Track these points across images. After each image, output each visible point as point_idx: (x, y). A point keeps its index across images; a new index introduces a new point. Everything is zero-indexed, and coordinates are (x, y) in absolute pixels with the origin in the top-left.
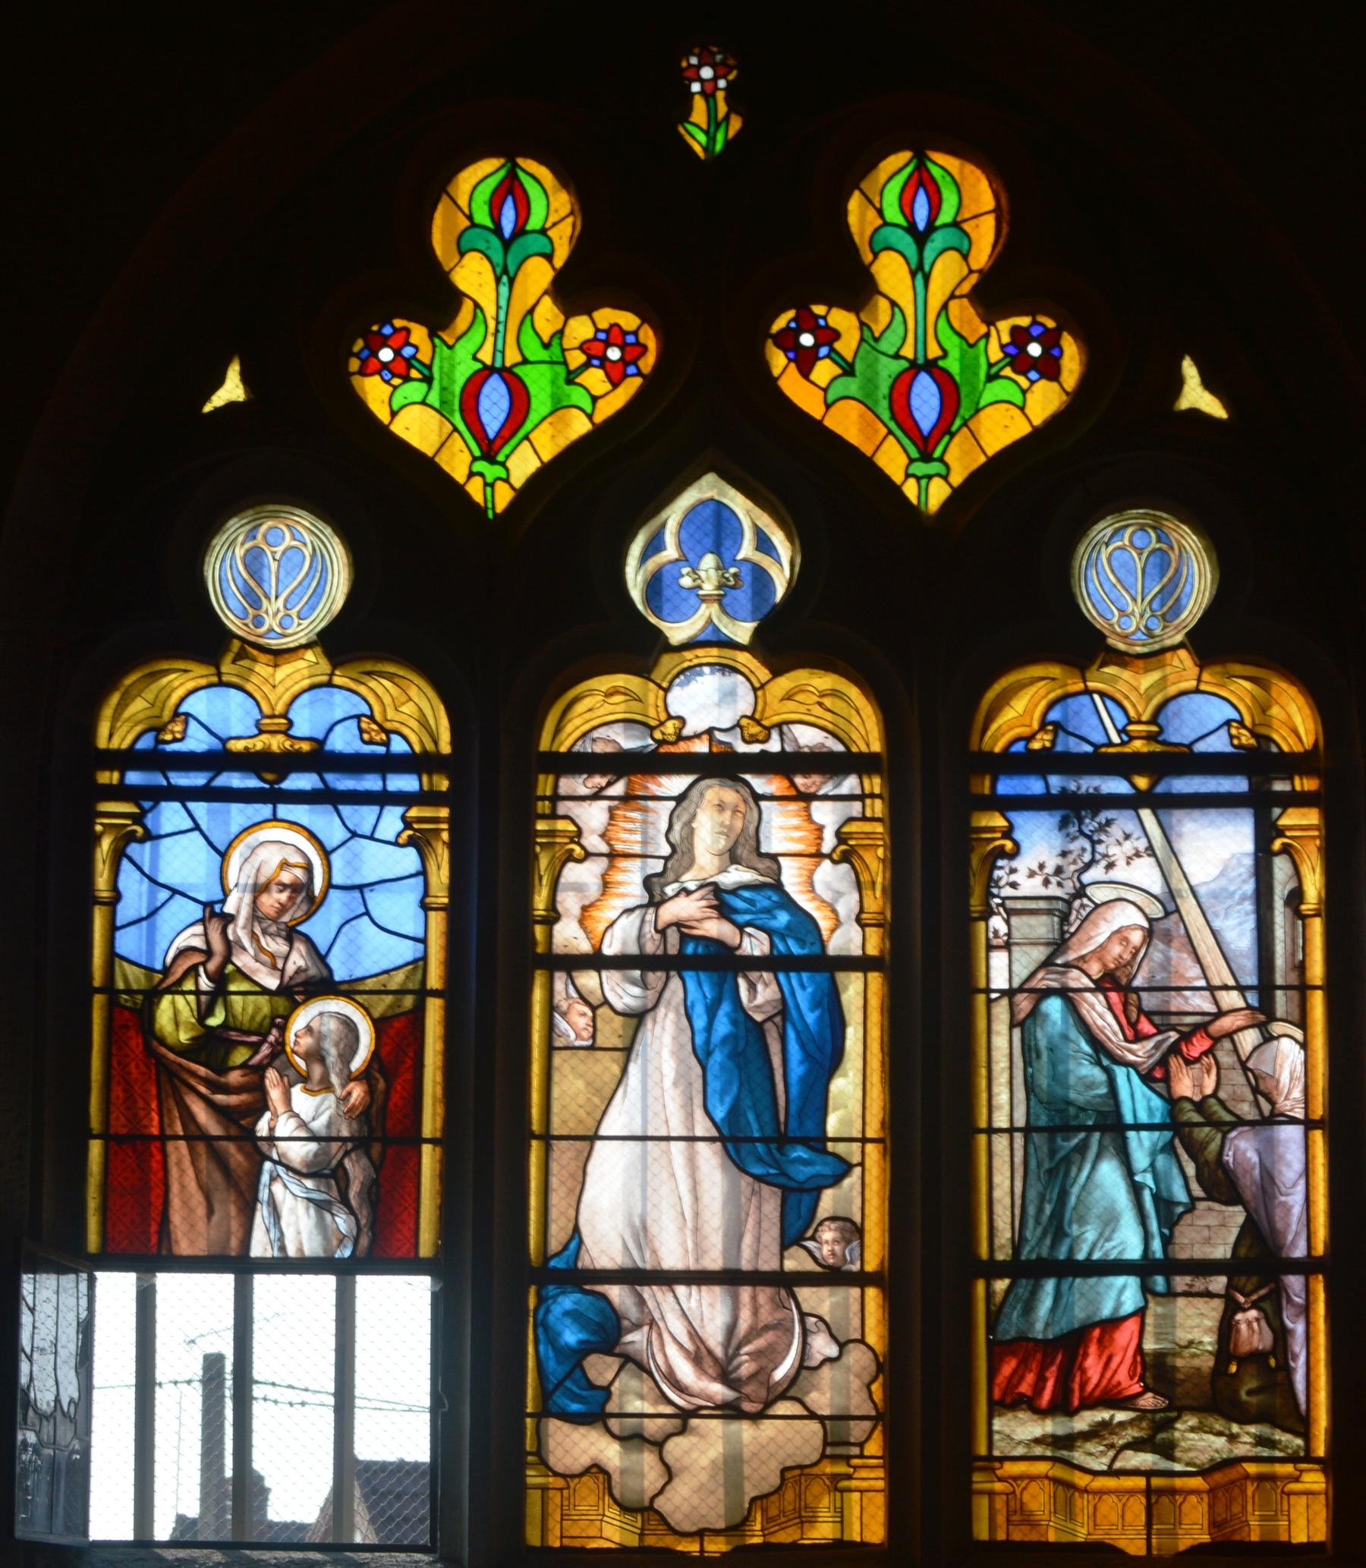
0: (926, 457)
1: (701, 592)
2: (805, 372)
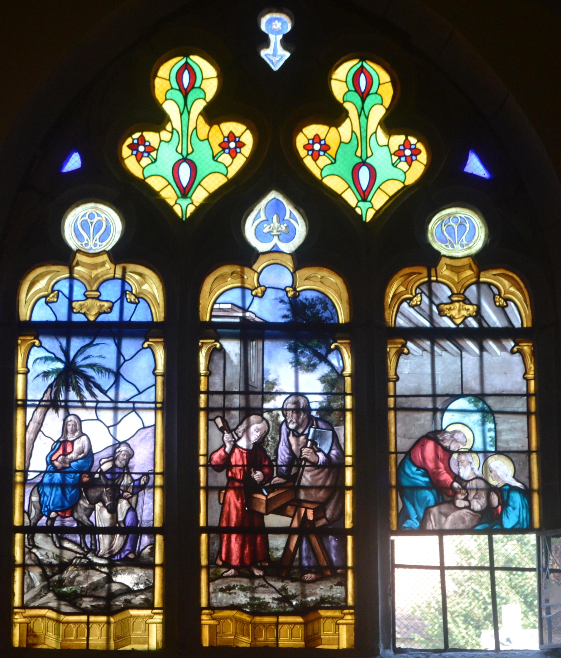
0: (364, 200)
1: (272, 234)
2: (315, 159)
